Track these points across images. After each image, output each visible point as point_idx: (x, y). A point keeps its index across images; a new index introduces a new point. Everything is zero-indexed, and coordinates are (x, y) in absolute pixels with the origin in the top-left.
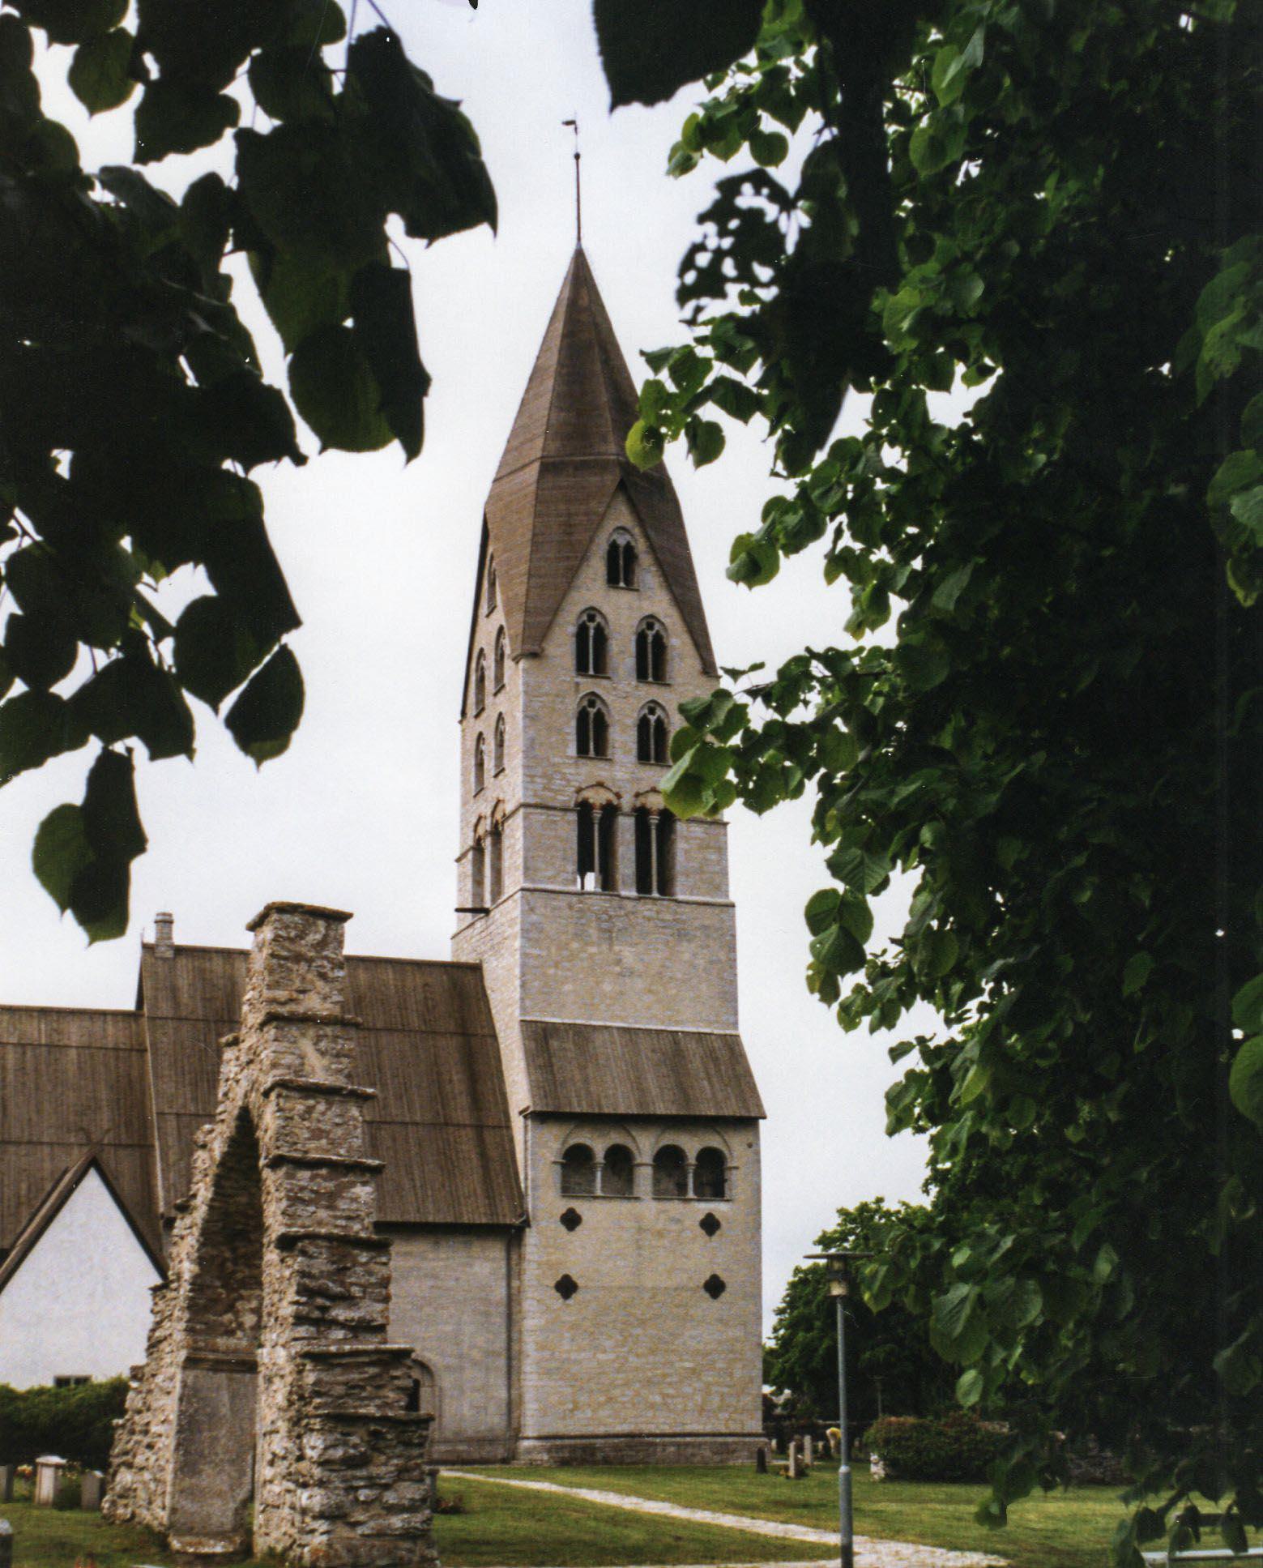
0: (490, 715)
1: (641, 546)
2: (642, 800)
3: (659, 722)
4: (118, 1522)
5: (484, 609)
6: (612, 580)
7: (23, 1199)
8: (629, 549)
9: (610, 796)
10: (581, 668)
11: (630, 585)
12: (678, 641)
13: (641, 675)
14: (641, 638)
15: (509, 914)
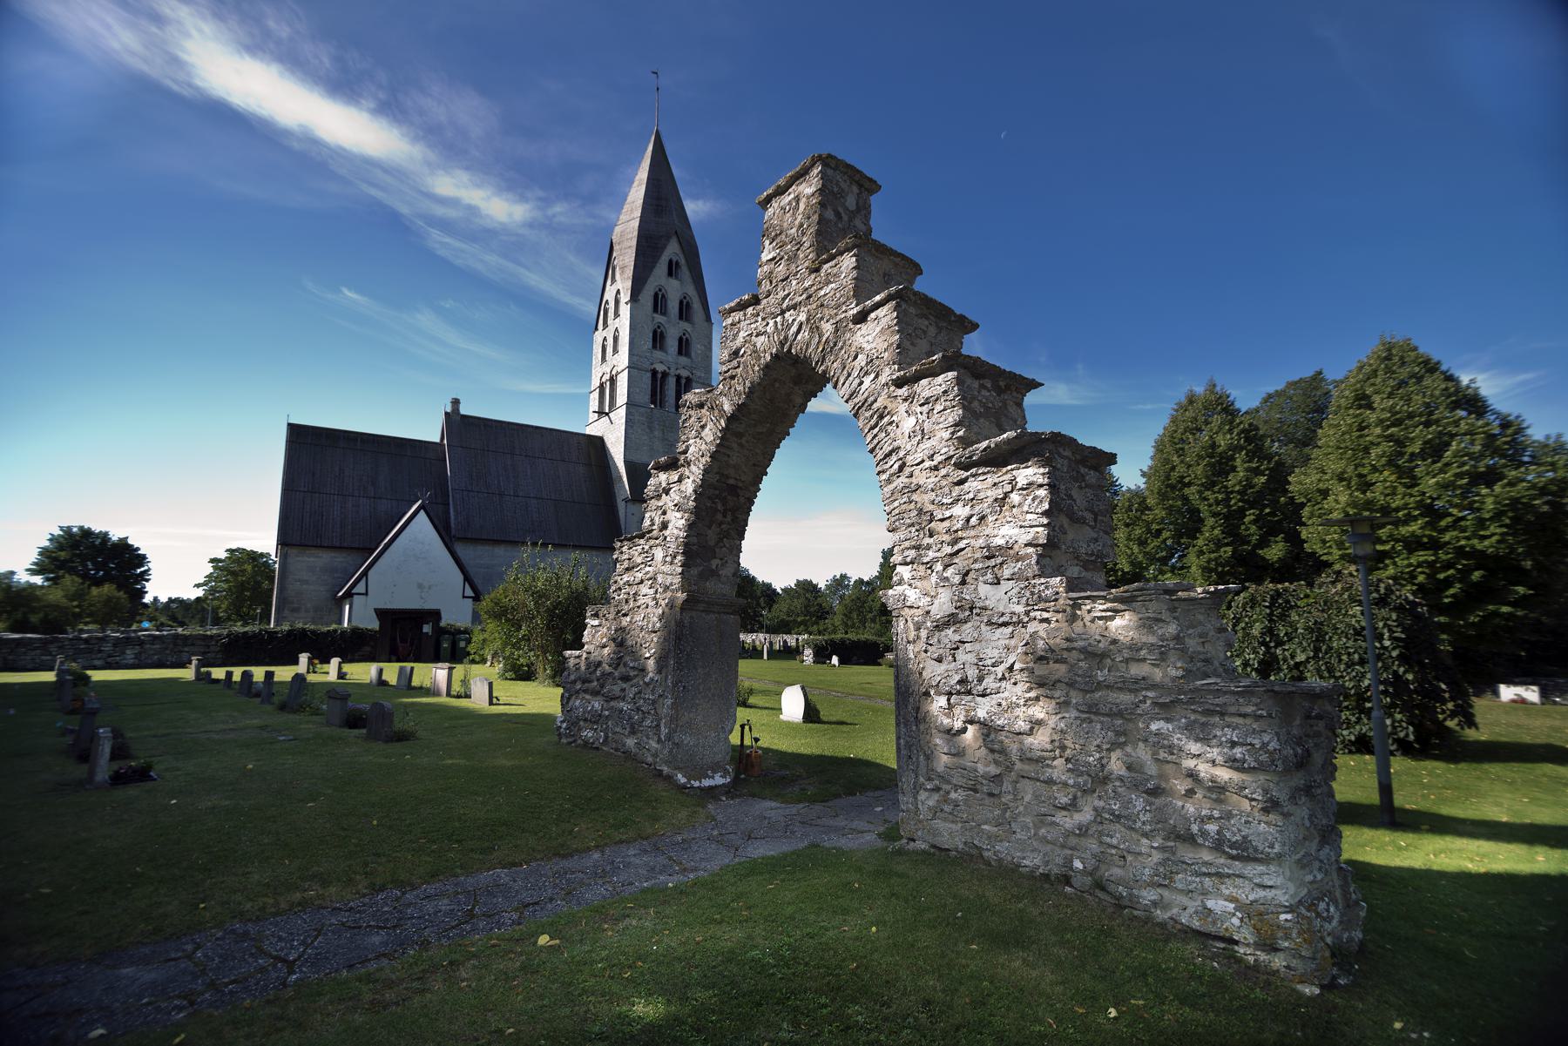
0: (611, 329)
1: (683, 262)
2: (678, 371)
3: (688, 303)
4: (579, 741)
5: (609, 282)
6: (670, 274)
7: (612, 703)
8: (677, 263)
9: (666, 368)
10: (655, 310)
11: (677, 278)
12: (696, 305)
13: (681, 318)
14: (681, 303)
15: (620, 415)
